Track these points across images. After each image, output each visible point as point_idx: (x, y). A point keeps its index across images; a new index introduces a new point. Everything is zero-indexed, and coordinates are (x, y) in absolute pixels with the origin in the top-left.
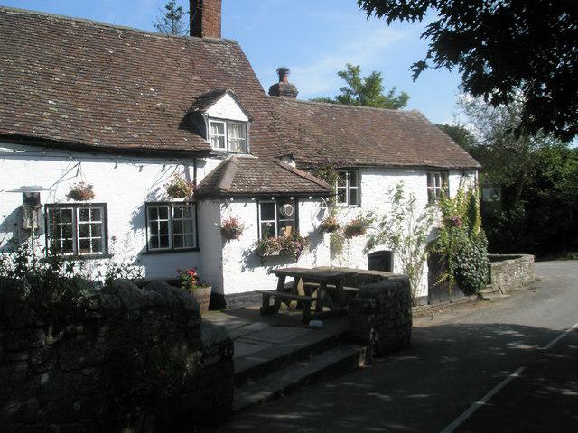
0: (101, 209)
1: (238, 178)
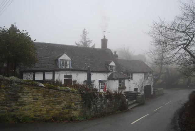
1: (115, 76)
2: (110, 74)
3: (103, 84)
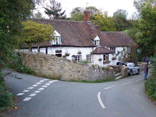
0: (81, 56)
2: (95, 48)
3: (77, 59)
